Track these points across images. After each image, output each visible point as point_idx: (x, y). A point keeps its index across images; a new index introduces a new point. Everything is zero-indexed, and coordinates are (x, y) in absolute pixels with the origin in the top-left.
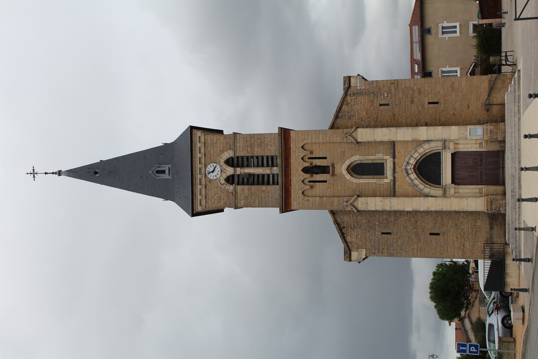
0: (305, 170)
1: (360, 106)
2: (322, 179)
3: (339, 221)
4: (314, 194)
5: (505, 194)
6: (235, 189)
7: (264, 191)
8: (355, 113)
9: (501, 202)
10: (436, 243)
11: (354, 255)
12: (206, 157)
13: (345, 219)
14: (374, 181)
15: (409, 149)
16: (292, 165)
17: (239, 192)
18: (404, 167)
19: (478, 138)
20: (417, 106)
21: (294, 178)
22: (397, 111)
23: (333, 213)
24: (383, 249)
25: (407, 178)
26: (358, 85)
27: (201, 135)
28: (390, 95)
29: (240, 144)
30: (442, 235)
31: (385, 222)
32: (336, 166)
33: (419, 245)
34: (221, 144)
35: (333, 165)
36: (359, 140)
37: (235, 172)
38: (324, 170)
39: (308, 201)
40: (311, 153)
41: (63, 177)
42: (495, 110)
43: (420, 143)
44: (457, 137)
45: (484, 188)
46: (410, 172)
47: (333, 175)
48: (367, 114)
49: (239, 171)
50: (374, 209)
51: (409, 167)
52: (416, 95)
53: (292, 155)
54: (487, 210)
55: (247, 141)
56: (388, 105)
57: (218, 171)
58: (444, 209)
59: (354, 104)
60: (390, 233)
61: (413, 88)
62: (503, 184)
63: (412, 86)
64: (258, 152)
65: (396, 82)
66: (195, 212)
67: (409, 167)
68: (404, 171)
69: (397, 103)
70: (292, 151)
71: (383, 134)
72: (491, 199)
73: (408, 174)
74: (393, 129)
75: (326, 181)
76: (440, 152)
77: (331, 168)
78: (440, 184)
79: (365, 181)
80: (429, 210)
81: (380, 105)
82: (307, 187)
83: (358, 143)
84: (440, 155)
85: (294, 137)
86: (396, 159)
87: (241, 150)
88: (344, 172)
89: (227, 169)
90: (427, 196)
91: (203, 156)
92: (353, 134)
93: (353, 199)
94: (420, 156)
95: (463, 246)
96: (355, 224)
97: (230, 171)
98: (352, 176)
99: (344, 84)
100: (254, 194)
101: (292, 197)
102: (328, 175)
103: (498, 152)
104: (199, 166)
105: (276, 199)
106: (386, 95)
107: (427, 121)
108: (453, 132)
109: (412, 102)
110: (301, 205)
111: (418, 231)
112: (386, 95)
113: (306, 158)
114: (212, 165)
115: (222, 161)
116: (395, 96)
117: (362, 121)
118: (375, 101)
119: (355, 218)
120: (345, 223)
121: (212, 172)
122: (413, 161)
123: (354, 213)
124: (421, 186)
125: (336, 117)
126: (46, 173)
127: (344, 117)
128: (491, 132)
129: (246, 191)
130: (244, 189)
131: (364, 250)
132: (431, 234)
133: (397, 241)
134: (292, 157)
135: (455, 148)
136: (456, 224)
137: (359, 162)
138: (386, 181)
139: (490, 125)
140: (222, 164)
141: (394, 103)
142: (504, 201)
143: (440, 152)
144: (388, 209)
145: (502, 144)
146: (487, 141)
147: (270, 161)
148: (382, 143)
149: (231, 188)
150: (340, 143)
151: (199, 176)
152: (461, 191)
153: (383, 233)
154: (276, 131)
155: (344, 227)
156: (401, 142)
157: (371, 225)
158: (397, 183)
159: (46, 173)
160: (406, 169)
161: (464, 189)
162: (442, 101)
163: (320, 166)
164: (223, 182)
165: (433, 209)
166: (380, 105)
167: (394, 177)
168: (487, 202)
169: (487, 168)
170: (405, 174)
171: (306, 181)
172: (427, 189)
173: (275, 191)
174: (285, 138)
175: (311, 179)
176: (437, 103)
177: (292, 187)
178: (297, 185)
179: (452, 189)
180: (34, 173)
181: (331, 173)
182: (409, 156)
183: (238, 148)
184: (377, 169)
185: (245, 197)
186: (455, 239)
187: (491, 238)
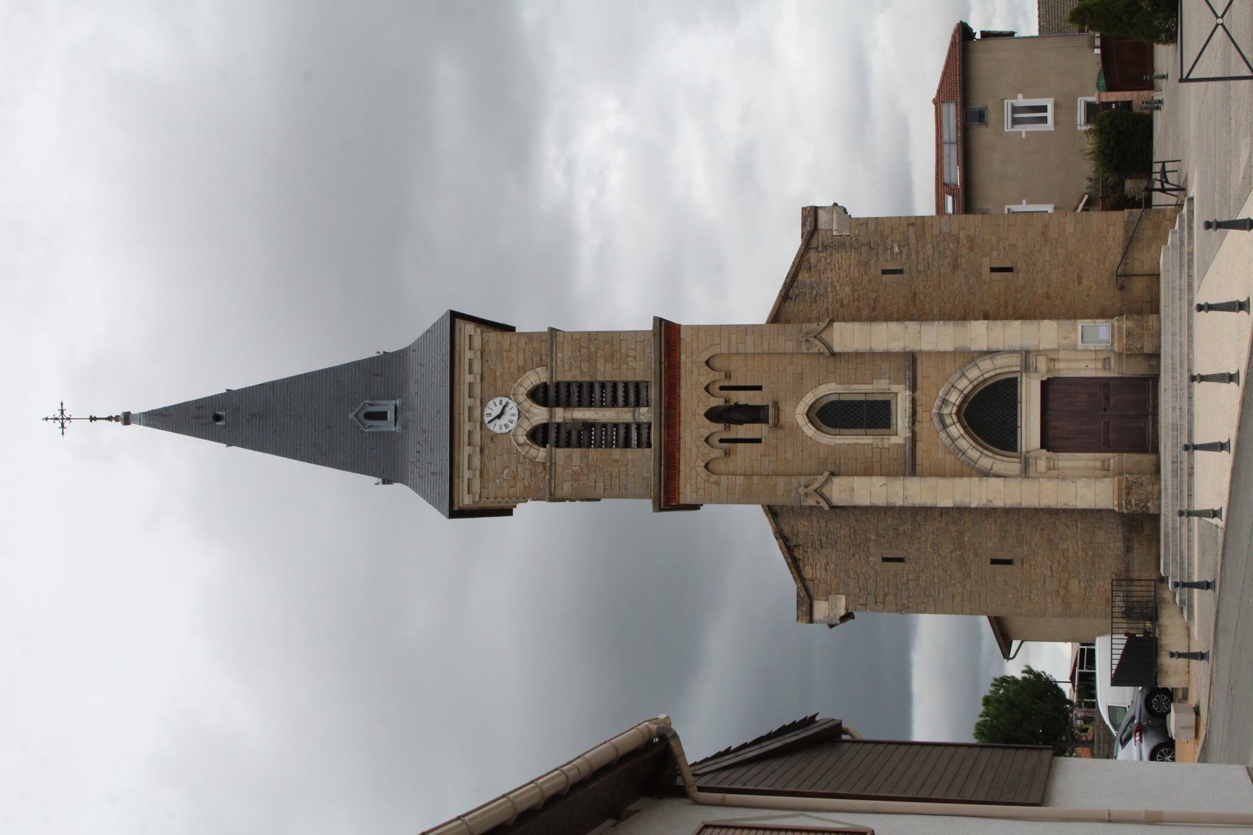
0: (714, 415)
1: (839, 272)
2: (750, 436)
3: (786, 530)
5: (1157, 471)
6: (550, 457)
7: (617, 461)
9: (1149, 488)
10: (1006, 582)
13: (801, 528)
14: (867, 440)
15: (948, 371)
16: (683, 404)
17: (559, 463)
18: (934, 411)
19: (1100, 346)
20: (966, 276)
24: (885, 595)
25: (943, 435)
26: (835, 226)
28: (905, 251)
29: (564, 353)
30: (1017, 563)
31: (891, 533)
32: (782, 407)
33: (968, 587)
35: (776, 404)
36: (837, 349)
37: (551, 416)
38: (755, 414)
39: (717, 483)
41: (134, 428)
42: (1138, 287)
43: (969, 357)
44: (1054, 346)
45: (1113, 458)
46: (948, 421)
47: (777, 425)
49: (560, 415)
51: (946, 411)
54: (1120, 505)
55: (581, 347)
56: (900, 272)
58: (1024, 505)
59: (825, 270)
60: (901, 560)
62: (1155, 450)
64: (605, 372)
65: (919, 222)
66: (456, 508)
67: (946, 411)
68: (935, 419)
69: (921, 268)
71: (889, 336)
72: (1127, 481)
73: (945, 427)
74: (913, 326)
75: (758, 441)
76: (1016, 379)
77: (771, 411)
78: (1015, 450)
79: (847, 442)
80: (990, 505)
81: (884, 272)
82: (716, 453)
83: (833, 354)
84: (1016, 385)
86: (918, 393)
87: (567, 368)
88: (801, 420)
90: (986, 474)
91: (478, 380)
92: (824, 335)
93: (821, 479)
94: (971, 387)
96: (823, 538)
97: (540, 414)
98: (818, 429)
99: (803, 225)
101: (682, 475)
102: (764, 426)
103: (1144, 379)
104: (468, 402)
106: (896, 250)
107: (988, 308)
108: (1045, 334)
109: (955, 267)
112: (896, 250)
114: (497, 400)
115: (522, 392)
116: (918, 252)
118: (872, 262)
119: (822, 524)
120: (801, 535)
121: (499, 417)
122: (955, 398)
124: (974, 454)
125: (786, 296)
126: (92, 419)
128: (1129, 334)
130: (570, 457)
131: (843, 597)
132: (994, 562)
133: (917, 578)
134: (683, 384)
135: (1049, 370)
136: (1050, 540)
137: (835, 398)
138: (894, 440)
139: (1127, 318)
140: (522, 398)
142: (1156, 487)
143: (1016, 379)
144: (899, 503)
145: (1154, 362)
146: (1120, 354)
147: (633, 394)
148: (887, 355)
149: (541, 453)
150: (793, 354)
151: (467, 426)
152: (1061, 464)
153: (885, 560)
154: (649, 326)
156: (929, 353)
157: (859, 541)
158: (920, 445)
159: (92, 419)
160: (940, 416)
161: (1067, 460)
163: (746, 406)
164: (522, 439)
165: (999, 503)
166: (884, 272)
167: (914, 433)
168: (1120, 489)
169: (1119, 414)
170: (938, 426)
171: (715, 440)
172: (986, 460)
174: (667, 342)
175: (725, 436)
176: (1009, 270)
177: (682, 452)
178: (694, 449)
179: (1042, 460)
181: (771, 421)
182: (947, 386)
184: (873, 415)
185: (575, 473)
186: (1049, 573)
187: (1127, 570)
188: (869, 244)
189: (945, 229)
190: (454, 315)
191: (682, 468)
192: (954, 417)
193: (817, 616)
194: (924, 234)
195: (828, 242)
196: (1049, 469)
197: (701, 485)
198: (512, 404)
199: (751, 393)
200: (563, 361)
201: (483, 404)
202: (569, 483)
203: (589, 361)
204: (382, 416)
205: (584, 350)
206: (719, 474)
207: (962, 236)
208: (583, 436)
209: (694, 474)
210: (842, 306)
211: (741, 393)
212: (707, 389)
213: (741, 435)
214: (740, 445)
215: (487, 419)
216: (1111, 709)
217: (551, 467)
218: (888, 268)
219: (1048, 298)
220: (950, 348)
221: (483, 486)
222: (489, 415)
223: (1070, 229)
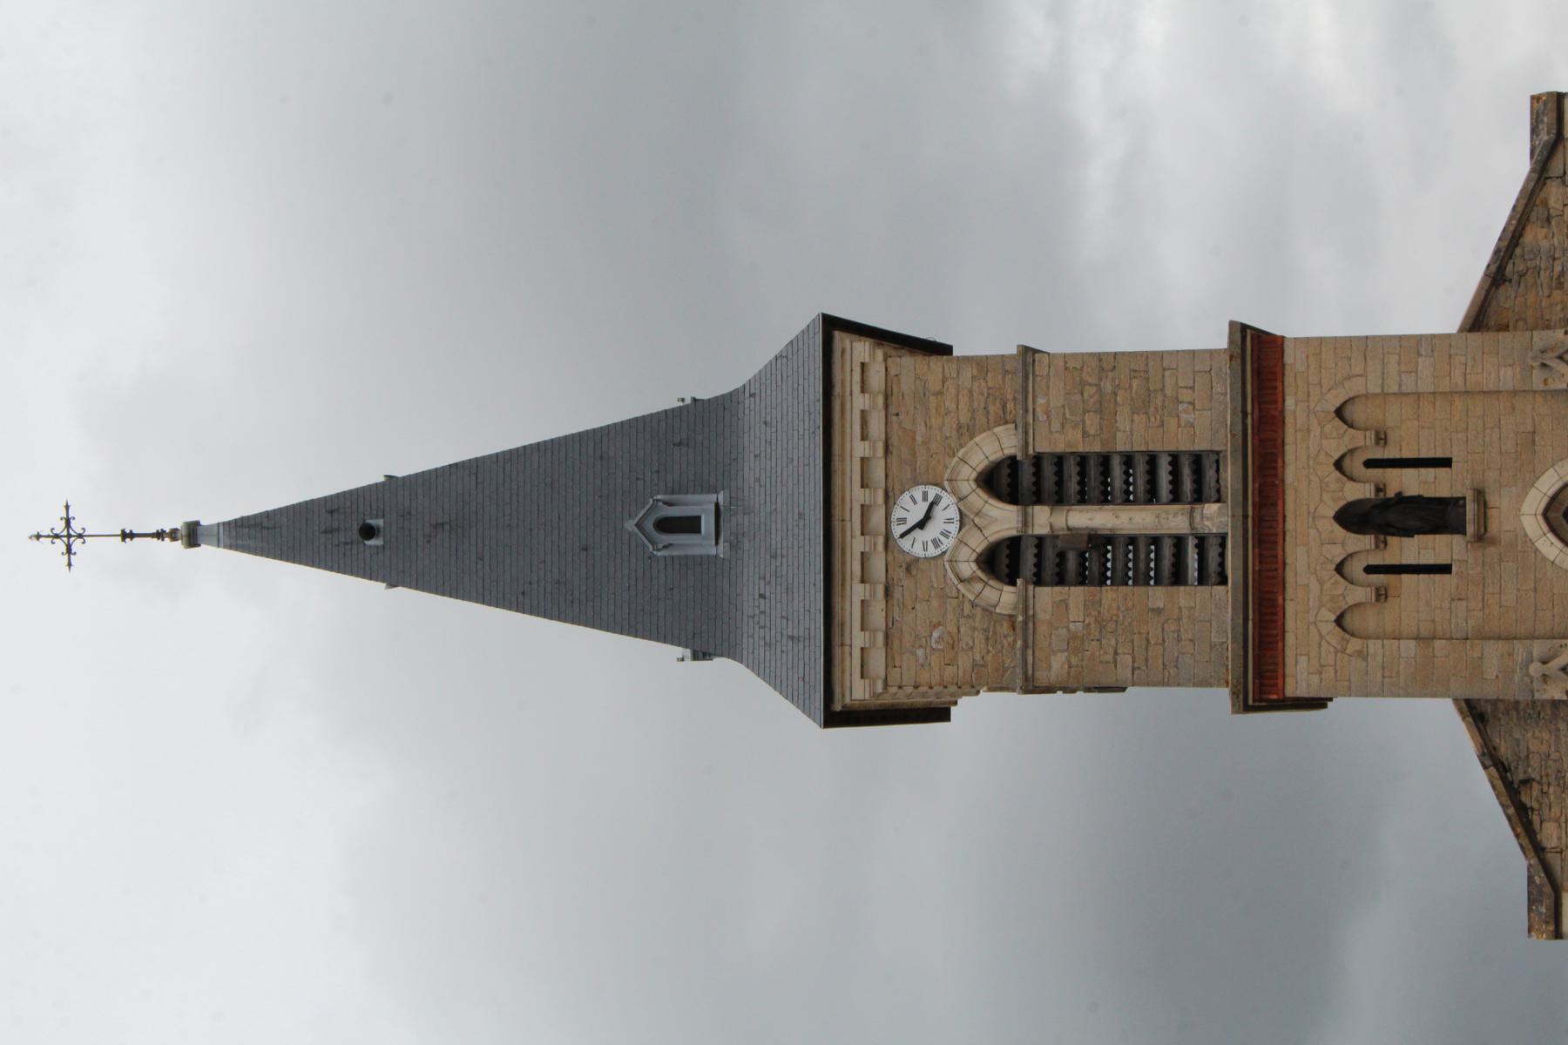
0: (1353, 518)
3: (1505, 751)
6: (1025, 604)
7: (1159, 611)
12: (894, 459)
17: (1041, 615)
21: (1301, 550)
23: (1476, 714)
27: (873, 356)
29: (1051, 397)
32: (1492, 500)
34: (964, 401)
35: (1480, 494)
37: (1025, 523)
38: (1438, 516)
39: (1363, 655)
40: (1381, 439)
41: (206, 551)
47: (1481, 538)
49: (1043, 519)
53: (1290, 450)
57: (949, 521)
64: (1132, 433)
66: (838, 707)
75: (1445, 569)
77: (1471, 509)
82: (1359, 594)
87: (1056, 425)
88: (1533, 525)
91: (880, 451)
97: (1002, 520)
99: (1534, 131)
100: (1111, 626)
101: (1290, 638)
102: (1457, 538)
113: (1356, 465)
114: (918, 492)
120: (1535, 761)
121: (921, 525)
125: (1497, 276)
129: (1076, 613)
140: (967, 486)
147: (1189, 477)
149: (1006, 597)
150: (1514, 393)
151: (858, 544)
154: (1221, 341)
155: (1527, 782)
163: (1418, 500)
164: (968, 568)
171: (1356, 568)
175: (1376, 559)
177: (1289, 593)
178: (1314, 586)
183: (1041, 416)
185: (1073, 637)
190: (831, 325)
191: (1290, 624)
198: (947, 499)
200: (1047, 413)
201: (889, 500)
202: (1062, 657)
203: (1100, 411)
205: (1089, 391)
212: (1338, 465)
215: (897, 530)
217: (1025, 623)
221: (890, 663)
222: (903, 521)
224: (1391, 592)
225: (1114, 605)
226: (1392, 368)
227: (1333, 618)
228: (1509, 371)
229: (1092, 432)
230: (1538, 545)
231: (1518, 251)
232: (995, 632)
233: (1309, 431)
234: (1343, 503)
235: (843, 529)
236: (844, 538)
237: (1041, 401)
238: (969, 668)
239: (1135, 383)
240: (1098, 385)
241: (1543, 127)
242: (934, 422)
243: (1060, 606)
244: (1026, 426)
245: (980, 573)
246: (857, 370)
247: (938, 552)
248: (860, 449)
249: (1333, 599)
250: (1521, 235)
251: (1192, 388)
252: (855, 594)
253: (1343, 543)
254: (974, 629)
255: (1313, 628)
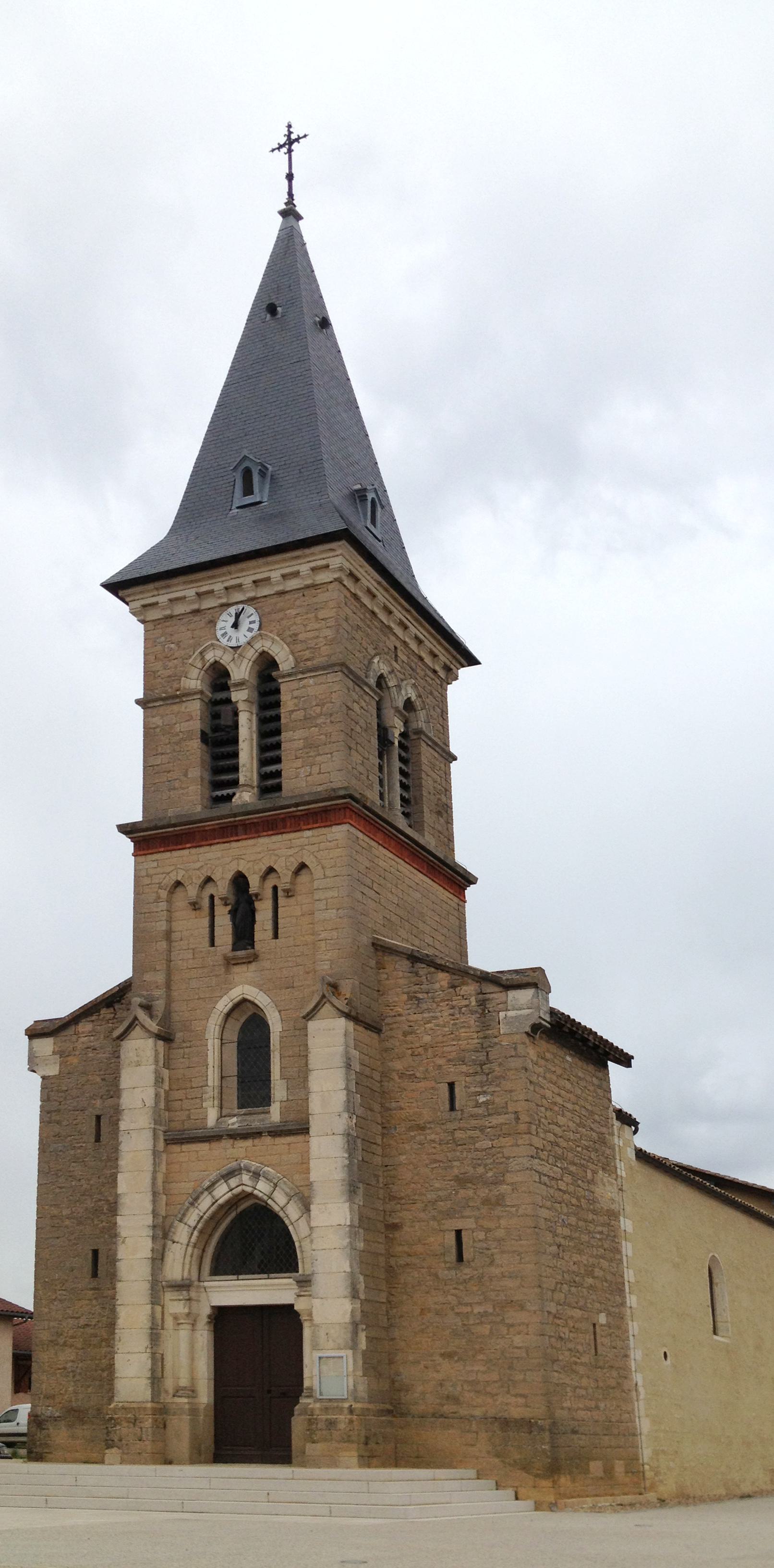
0: (240, 881)
2: (218, 931)
4: (177, 915)
6: (188, 694)
7: (186, 775)
8: (429, 1010)
11: (46, 1046)
14: (213, 1078)
16: (251, 842)
17: (183, 707)
20: (448, 1198)
21: (219, 854)
22: (433, 1137)
24: (58, 1122)
26: (511, 1013)
28: (480, 1111)
30: (94, 1284)
32: (253, 966)
33: (67, 1222)
38: (244, 935)
39: (158, 899)
40: (289, 894)
46: (233, 1182)
47: (230, 963)
48: (425, 1047)
50: (123, 1085)
51: (246, 1178)
52: (483, 1192)
56: (452, 1108)
60: (98, 1140)
61: (503, 1182)
63: (509, 1178)
67: (246, 1178)
68: (234, 1164)
70: (292, 835)
75: (212, 944)
79: (210, 1053)
81: (451, 1086)
82: (192, 892)
85: (329, 837)
86: (268, 1140)
87: (296, 693)
88: (236, 993)
89: (245, 661)
95: (65, 1344)
97: (241, 671)
98: (228, 1015)
100: (177, 748)
101: (168, 854)
102: (230, 947)
105: (166, 810)
106: (482, 1099)
107: (406, 1229)
109: (462, 1181)
110: (147, 881)
111: (103, 1217)
112: (482, 1099)
117: (405, 1034)
118: (464, 1068)
122: (262, 1188)
123: (111, 1032)
124: (192, 1218)
126: (290, 177)
127: (414, 979)
129: (184, 726)
130: (191, 718)
132: (95, 1253)
140: (258, 646)
141: (455, 1125)
144: (123, 1126)
147: (270, 783)
158: (204, 1147)
159: (290, 177)
161: (204, 1338)
162: (467, 1271)
163: (253, 921)
164: (210, 657)
166: (451, 1086)
169: (253, 1405)
170: (224, 1171)
172: (183, 1233)
173: (191, 798)
174: (326, 811)
176: (460, 1258)
177: (193, 851)
178: (198, 865)
180: (290, 142)
186: (82, 1322)
188: (488, 1061)
189: (513, 1165)
191: (176, 854)
192: (240, 1189)
193: (37, 1042)
194: (505, 1135)
195: (490, 1006)
196: (176, 1318)
197: (156, 880)
199: (269, 926)
200: (304, 687)
201: (251, 601)
202: (160, 723)
203: (306, 719)
204: (248, 490)
205: (318, 710)
206: (169, 901)
207: (504, 1188)
208: (220, 740)
209: (168, 869)
210: (405, 1034)
211: (269, 914)
213: (218, 921)
214: (206, 922)
216: (16, 1410)
217: (177, 697)
218: (457, 1090)
219: (423, 1312)
220: (313, 1176)
223: (518, 1340)
224: (198, 912)
225: (190, 748)
226: (330, 894)
227: (179, 879)
228: (326, 966)
229: (293, 716)
230: (225, 998)
231: (433, 970)
232: (173, 680)
233: (290, 848)
234: (247, 875)
235: (224, 575)
236: (220, 576)
237: (311, 681)
238: (154, 669)
239: (323, 737)
240: (321, 714)
241: (514, 976)
242: (298, 620)
243: (192, 716)
244: (295, 674)
245: (208, 664)
246: (324, 562)
247: (219, 636)
248: (275, 575)
249: (190, 878)
250: (443, 971)
251: (319, 773)
252: (187, 590)
253: (223, 878)
254: (176, 667)
255: (173, 868)
